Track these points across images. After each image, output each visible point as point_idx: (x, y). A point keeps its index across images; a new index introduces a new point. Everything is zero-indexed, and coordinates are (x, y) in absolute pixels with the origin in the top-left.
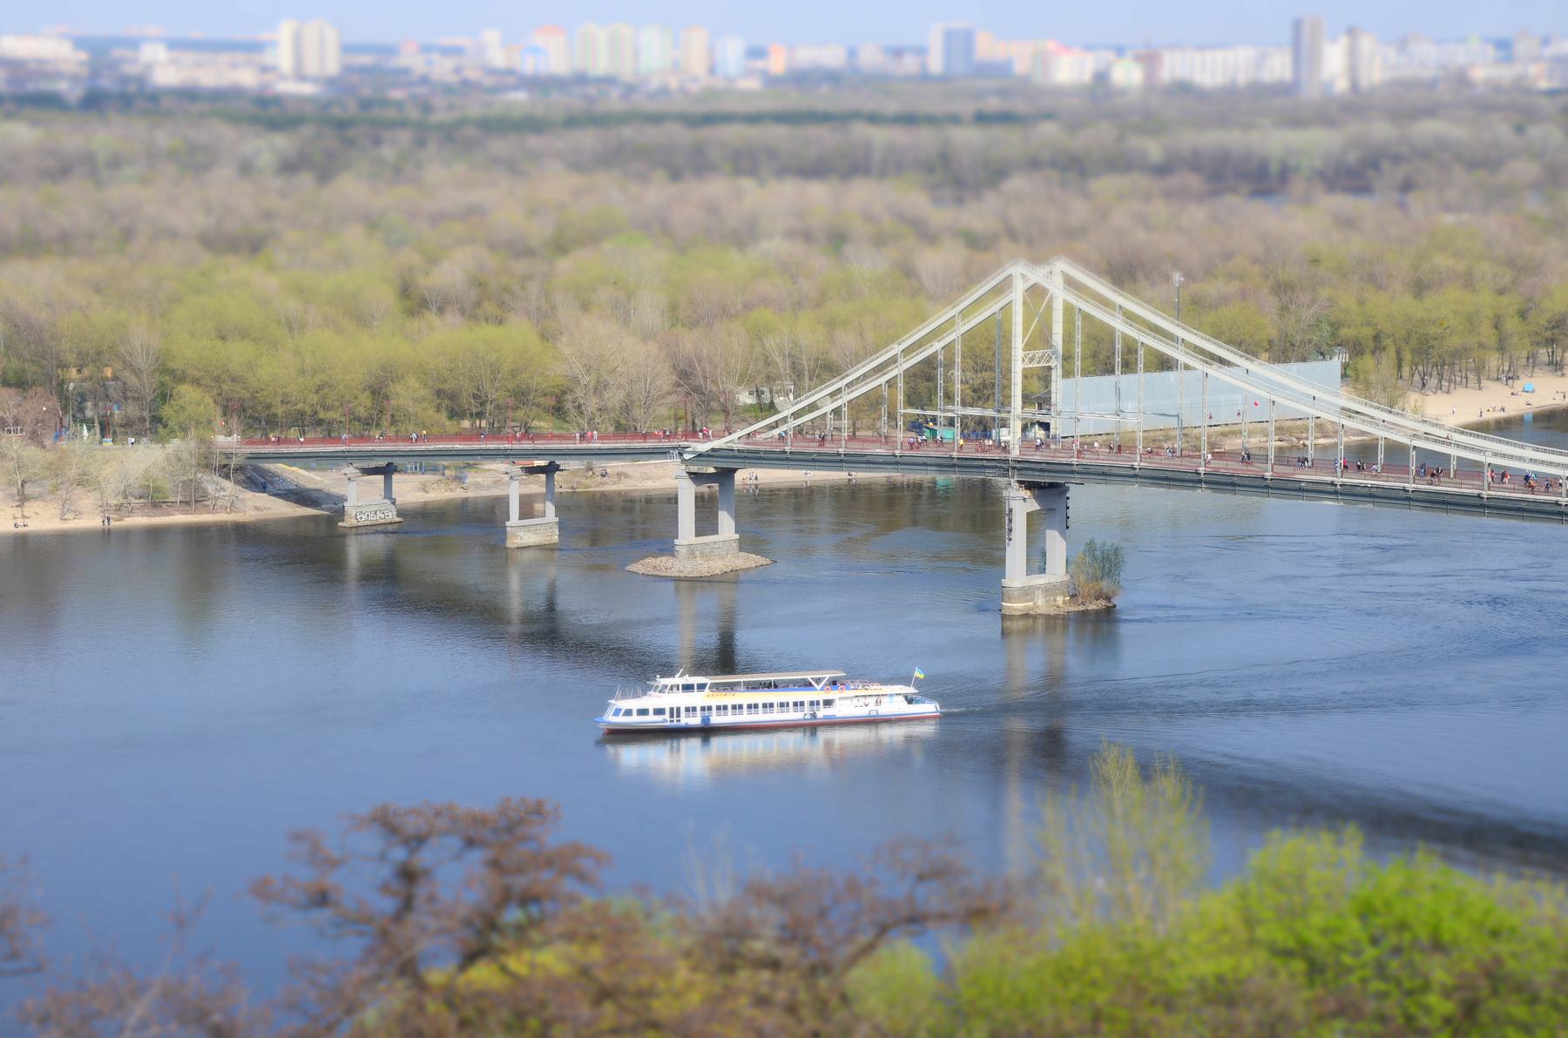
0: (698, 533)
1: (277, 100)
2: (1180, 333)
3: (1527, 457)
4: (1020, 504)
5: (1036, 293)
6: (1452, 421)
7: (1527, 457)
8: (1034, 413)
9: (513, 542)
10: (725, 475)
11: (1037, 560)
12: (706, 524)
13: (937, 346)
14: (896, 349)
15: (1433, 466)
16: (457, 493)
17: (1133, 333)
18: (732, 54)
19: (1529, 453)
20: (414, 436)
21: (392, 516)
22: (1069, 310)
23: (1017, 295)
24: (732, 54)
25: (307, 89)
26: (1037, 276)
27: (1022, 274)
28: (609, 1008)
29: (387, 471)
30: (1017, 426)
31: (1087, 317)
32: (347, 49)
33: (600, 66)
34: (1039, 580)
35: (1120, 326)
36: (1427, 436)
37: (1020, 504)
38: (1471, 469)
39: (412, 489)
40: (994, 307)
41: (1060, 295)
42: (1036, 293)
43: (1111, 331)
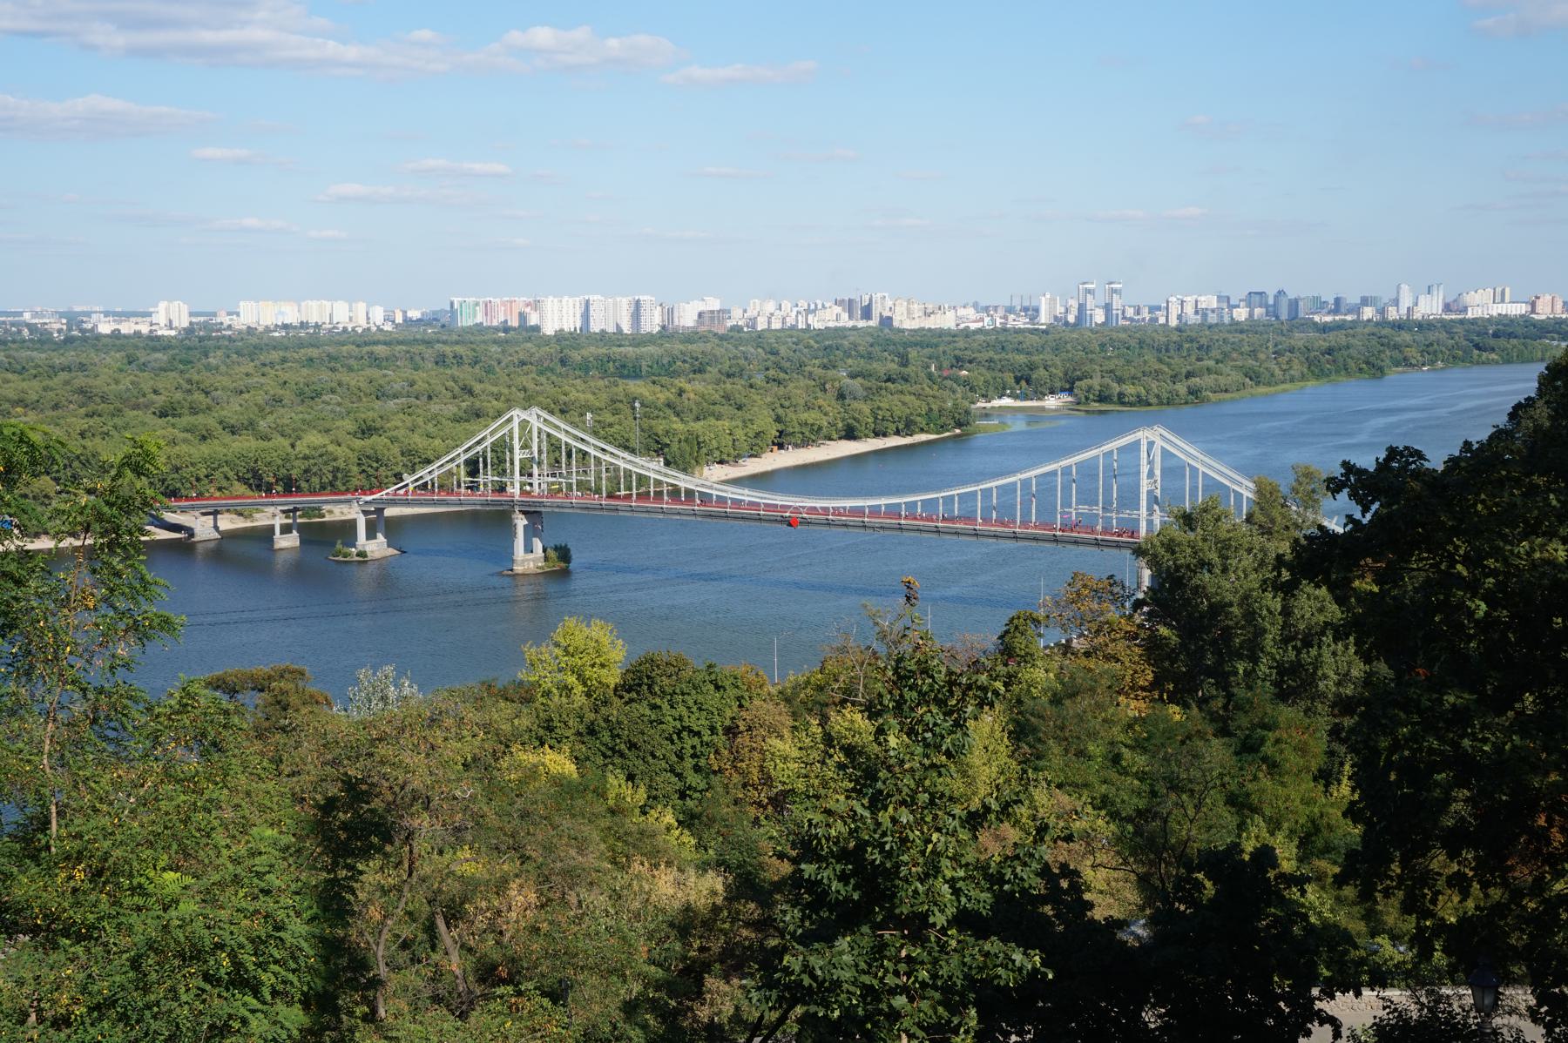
0: (367, 539)
1: (158, 338)
2: (563, 426)
3: (747, 495)
4: (521, 522)
5: (524, 424)
6: (715, 479)
7: (747, 495)
8: (524, 479)
9: (277, 546)
10: (380, 511)
11: (529, 549)
12: (371, 535)
13: (479, 448)
14: (460, 450)
15: (705, 498)
16: (249, 524)
17: (629, 467)
18: (378, 316)
19: (746, 491)
20: (1137, 728)
21: (217, 536)
22: (539, 429)
23: (516, 424)
24: (378, 316)
25: (173, 333)
26: (524, 415)
27: (517, 414)
28: (1105, 786)
29: (215, 513)
30: (517, 485)
31: (549, 435)
32: (191, 314)
33: (313, 319)
34: (531, 556)
35: (564, 438)
36: (703, 486)
37: (521, 522)
38: (722, 500)
39: (227, 523)
40: (505, 430)
41: (536, 424)
42: (524, 424)
43: (559, 440)
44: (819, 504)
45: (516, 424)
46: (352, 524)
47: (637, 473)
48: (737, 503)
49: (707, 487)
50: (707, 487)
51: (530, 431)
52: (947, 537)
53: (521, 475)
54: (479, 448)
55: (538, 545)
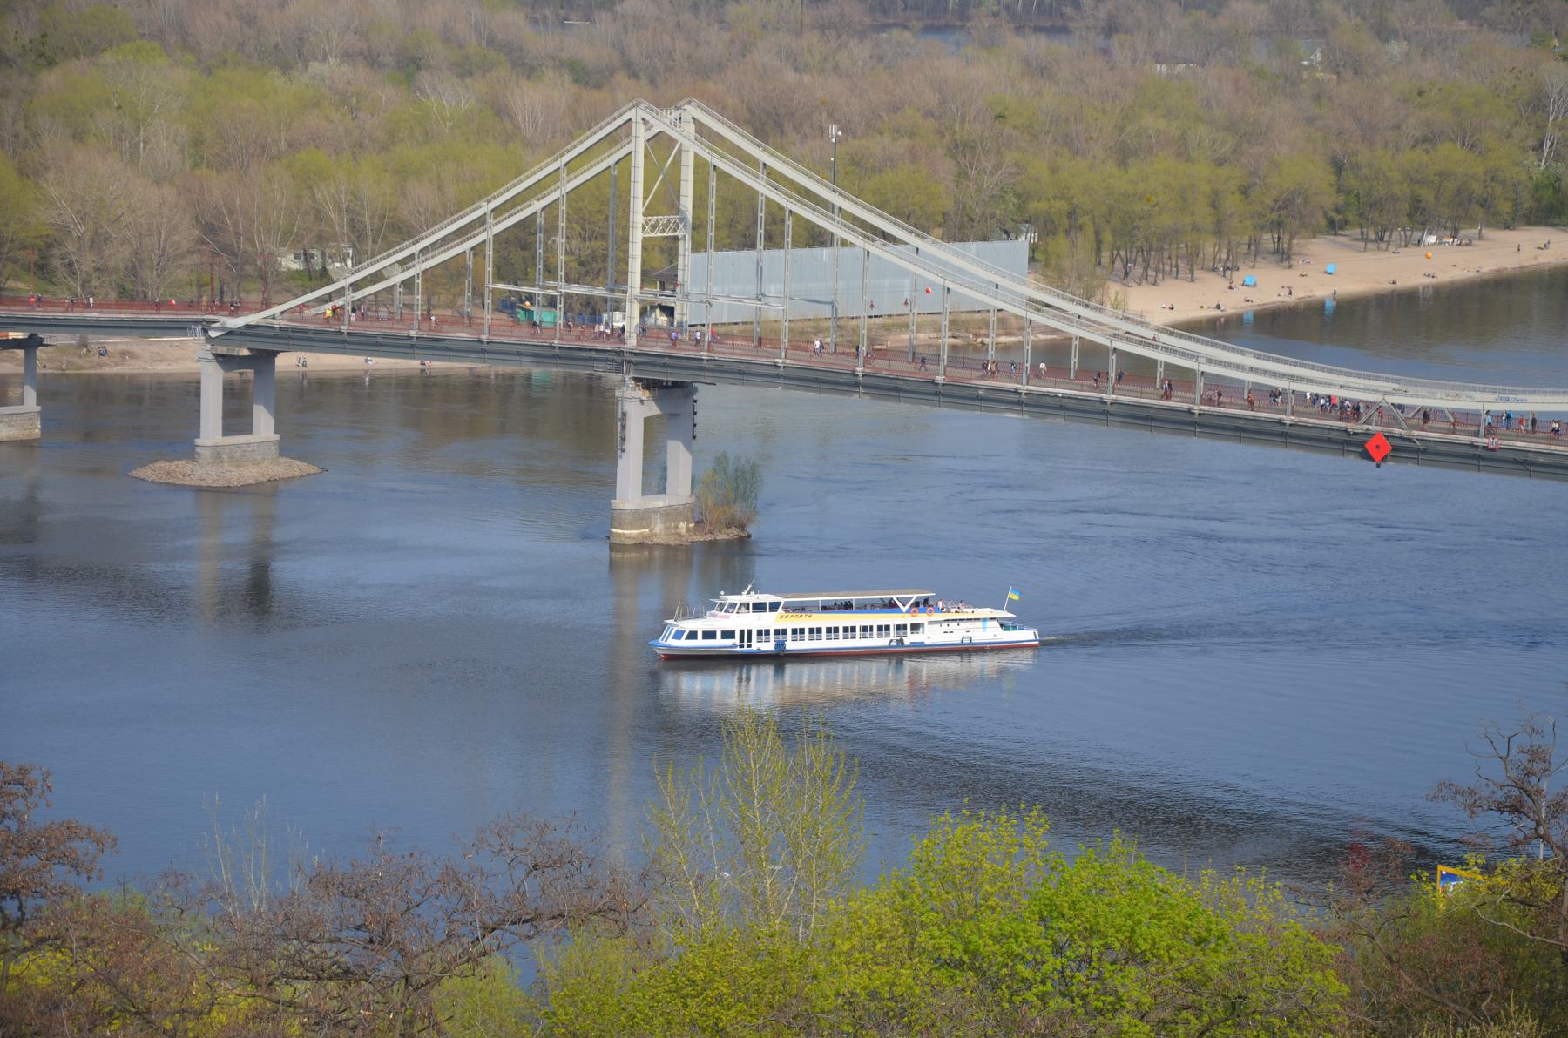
5: (660, 143)
6: (1161, 318)
8: (654, 294)
11: (655, 479)
12: (236, 418)
14: (486, 208)
15: (1138, 370)
22: (700, 164)
23: (641, 135)
26: (662, 123)
27: (644, 120)
30: (634, 310)
31: (723, 176)
34: (659, 502)
36: (1129, 337)
37: (637, 407)
38: (1180, 378)
41: (691, 148)
42: (660, 143)
44: (1420, 397)
45: (641, 135)
46: (191, 389)
47: (1167, 365)
48: (1219, 388)
49: (1142, 342)
50: (1142, 342)
51: (677, 162)
52: (825, 300)
53: (472, 249)
54: (537, 206)
55: (680, 461)
